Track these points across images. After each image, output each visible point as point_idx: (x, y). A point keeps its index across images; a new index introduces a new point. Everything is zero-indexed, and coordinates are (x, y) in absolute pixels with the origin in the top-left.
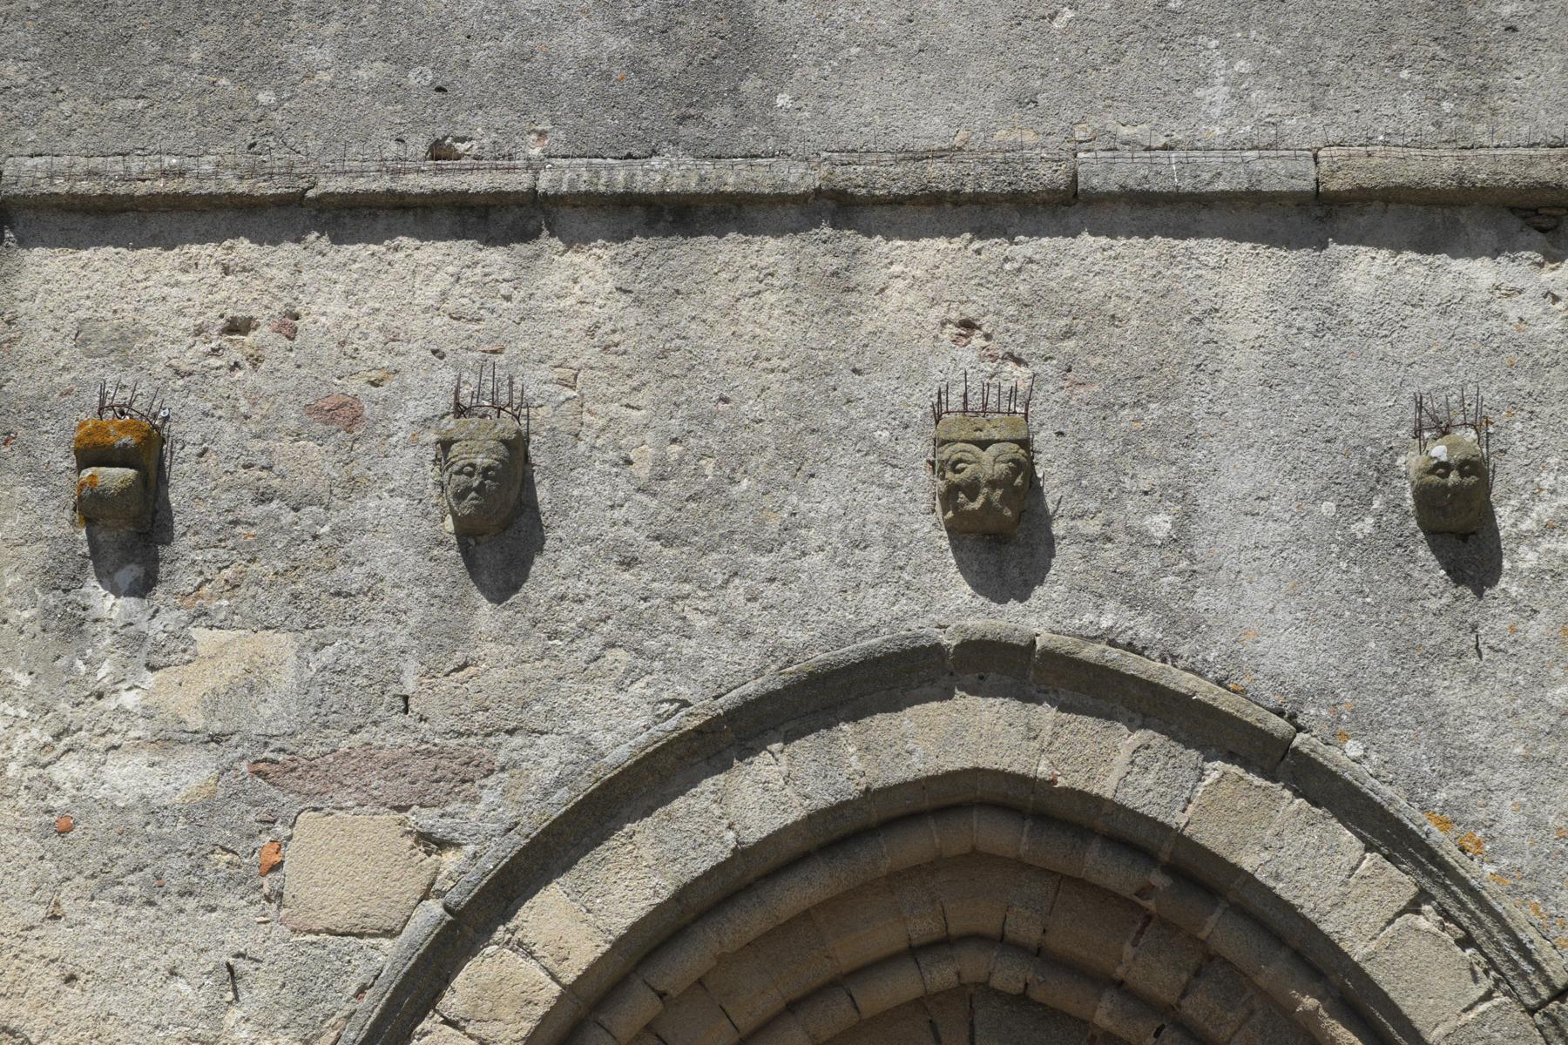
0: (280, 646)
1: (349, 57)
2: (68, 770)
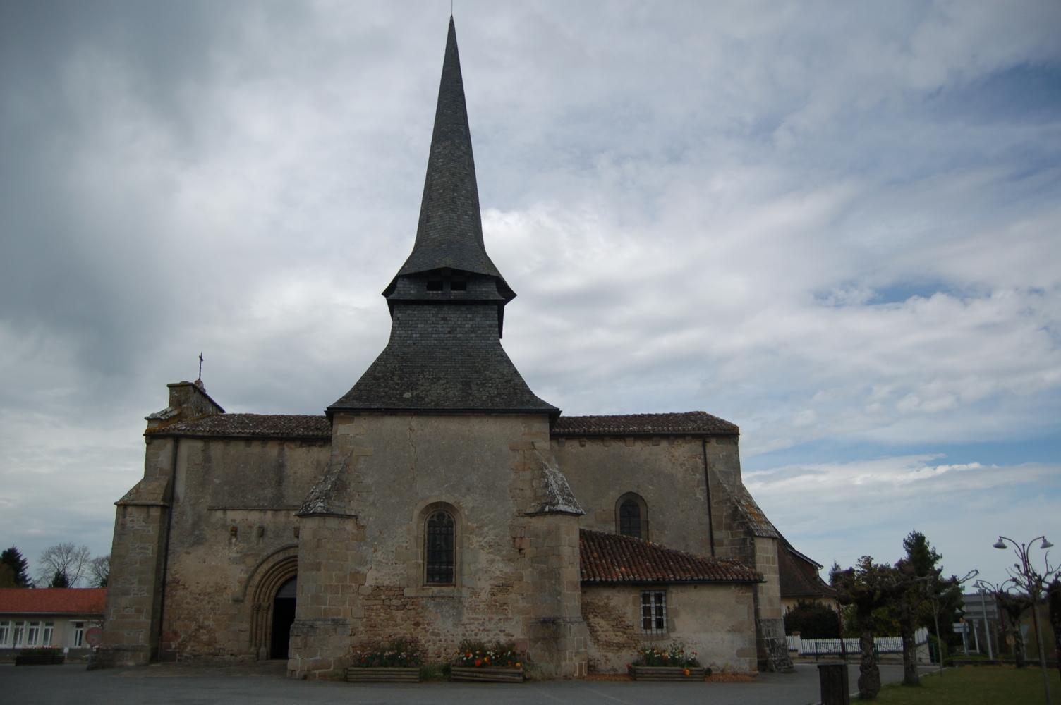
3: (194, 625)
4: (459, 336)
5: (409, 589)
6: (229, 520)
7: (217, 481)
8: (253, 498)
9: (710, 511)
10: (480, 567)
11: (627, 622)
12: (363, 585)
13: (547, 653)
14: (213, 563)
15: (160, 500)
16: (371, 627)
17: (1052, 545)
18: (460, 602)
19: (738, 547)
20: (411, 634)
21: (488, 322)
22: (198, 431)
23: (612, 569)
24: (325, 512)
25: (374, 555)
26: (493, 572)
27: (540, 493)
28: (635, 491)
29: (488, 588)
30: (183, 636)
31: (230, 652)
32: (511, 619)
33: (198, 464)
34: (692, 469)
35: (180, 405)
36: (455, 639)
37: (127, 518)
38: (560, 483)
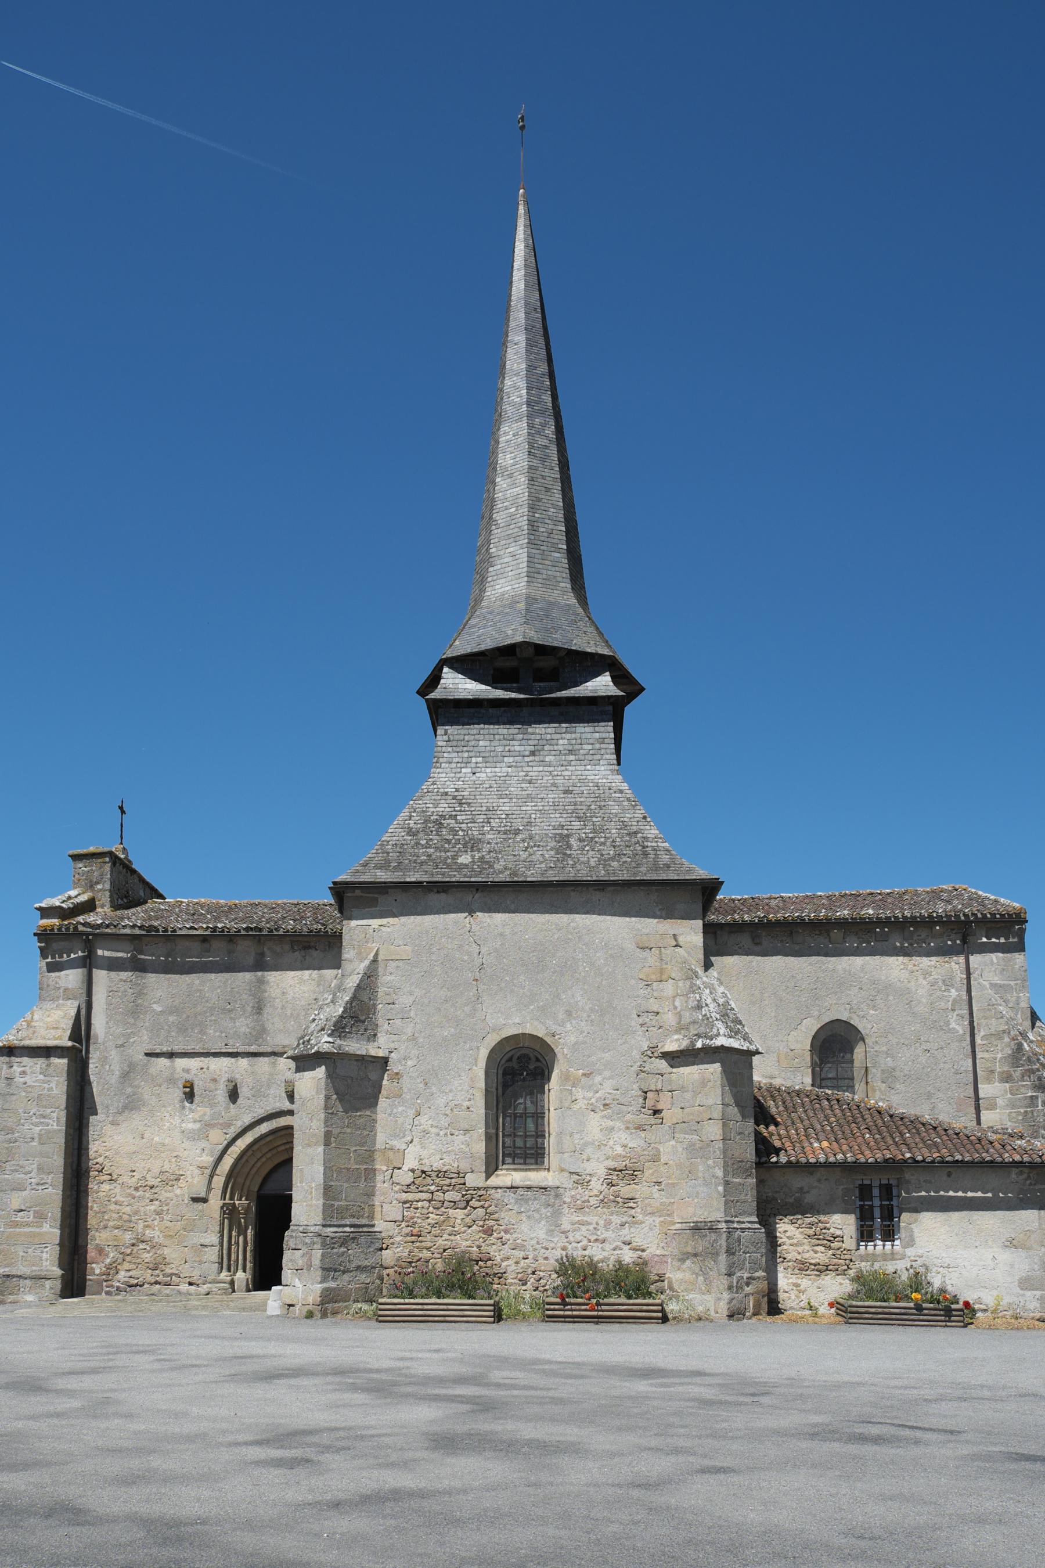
0: (208, 1110)
1: (215, 1032)
2: (183, 1125)
3: (128, 1237)
4: (547, 759)
6: (179, 1070)
7: (158, 1008)
8: (217, 1034)
9: (974, 1052)
11: (832, 1230)
12: (399, 1168)
13: (701, 1278)
14: (156, 1139)
15: (67, 1038)
16: (412, 1235)
17: (69, 856)
18: (557, 1196)
19: (1022, 1111)
20: (479, 1247)
21: (597, 735)
22: (124, 927)
23: (806, 1144)
25: (416, 1122)
26: (611, 1148)
27: (687, 1017)
29: (602, 1172)
30: (112, 1255)
31: (188, 1280)
32: (642, 1222)
34: (944, 981)
35: (91, 887)
36: (550, 1256)
38: (721, 1001)
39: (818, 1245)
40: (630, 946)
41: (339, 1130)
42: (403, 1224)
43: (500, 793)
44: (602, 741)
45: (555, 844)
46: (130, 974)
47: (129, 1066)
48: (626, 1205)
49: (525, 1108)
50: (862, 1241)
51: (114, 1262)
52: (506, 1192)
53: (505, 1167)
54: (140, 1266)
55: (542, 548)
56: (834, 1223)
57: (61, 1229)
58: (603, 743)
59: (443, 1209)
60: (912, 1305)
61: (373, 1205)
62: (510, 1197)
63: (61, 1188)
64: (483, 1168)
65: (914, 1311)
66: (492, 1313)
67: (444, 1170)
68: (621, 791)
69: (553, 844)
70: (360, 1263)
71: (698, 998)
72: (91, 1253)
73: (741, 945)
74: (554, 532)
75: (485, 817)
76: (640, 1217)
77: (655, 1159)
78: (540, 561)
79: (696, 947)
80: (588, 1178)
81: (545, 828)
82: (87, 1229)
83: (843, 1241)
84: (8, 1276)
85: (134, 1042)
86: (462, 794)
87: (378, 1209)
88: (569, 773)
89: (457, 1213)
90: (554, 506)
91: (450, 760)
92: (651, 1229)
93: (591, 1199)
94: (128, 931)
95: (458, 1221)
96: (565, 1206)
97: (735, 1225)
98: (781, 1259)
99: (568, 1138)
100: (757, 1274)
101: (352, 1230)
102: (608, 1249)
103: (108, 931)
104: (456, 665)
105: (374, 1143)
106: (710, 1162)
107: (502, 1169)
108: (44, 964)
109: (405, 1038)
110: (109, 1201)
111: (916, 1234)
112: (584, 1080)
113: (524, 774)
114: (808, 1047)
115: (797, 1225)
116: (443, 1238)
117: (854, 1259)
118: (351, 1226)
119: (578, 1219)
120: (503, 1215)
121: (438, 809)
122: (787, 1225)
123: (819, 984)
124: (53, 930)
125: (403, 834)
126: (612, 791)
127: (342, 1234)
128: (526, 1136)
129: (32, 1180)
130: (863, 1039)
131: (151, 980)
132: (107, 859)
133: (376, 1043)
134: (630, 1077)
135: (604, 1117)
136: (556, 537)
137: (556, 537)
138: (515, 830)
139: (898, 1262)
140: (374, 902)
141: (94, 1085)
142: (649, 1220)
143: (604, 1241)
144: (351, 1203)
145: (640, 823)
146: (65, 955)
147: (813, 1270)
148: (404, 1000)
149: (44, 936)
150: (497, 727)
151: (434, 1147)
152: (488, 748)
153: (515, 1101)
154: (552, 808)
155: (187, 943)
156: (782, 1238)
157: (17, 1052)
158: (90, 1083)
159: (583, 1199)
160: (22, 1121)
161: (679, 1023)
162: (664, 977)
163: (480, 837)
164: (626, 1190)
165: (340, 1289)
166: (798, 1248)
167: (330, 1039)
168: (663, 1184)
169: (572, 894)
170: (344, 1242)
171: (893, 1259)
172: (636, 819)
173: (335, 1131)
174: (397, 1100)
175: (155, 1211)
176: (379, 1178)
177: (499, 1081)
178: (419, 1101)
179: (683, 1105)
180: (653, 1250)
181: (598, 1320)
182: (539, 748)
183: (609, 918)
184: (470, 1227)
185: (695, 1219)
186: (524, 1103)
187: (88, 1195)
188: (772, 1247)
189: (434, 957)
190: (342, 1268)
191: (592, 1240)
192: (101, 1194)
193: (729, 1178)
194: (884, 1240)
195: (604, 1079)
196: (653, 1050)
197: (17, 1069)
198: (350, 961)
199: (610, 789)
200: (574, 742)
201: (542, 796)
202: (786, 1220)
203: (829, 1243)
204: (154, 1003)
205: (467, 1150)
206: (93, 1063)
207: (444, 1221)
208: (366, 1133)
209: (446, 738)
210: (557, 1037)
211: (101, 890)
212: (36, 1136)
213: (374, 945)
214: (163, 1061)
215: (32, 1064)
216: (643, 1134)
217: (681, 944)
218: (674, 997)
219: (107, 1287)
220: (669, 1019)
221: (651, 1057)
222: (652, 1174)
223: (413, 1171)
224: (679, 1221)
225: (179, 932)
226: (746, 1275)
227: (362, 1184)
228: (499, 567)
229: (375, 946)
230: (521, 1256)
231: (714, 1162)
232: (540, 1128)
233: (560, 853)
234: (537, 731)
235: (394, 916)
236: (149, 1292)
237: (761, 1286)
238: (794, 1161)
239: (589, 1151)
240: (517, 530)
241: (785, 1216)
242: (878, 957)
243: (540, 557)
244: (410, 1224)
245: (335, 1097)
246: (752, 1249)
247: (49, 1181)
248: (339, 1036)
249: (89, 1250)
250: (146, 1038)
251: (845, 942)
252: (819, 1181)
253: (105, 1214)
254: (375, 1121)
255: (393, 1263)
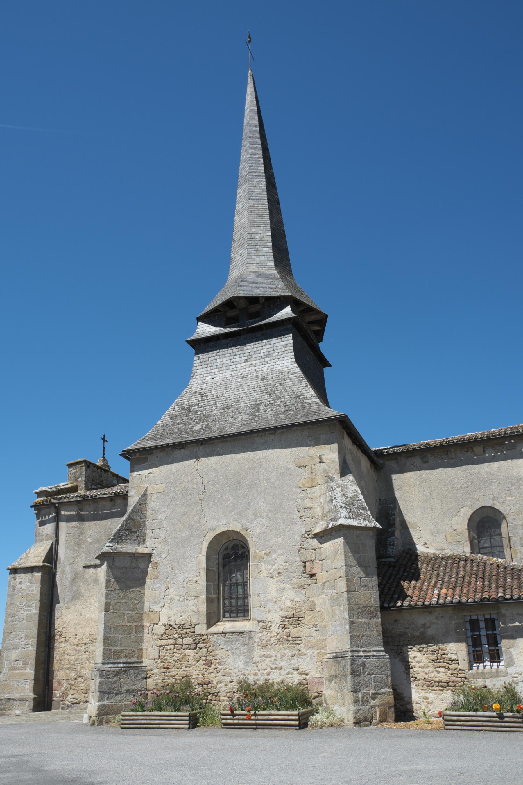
3: (73, 674)
4: (254, 362)
5: (200, 626)
7: (89, 540)
10: (270, 597)
11: (449, 655)
12: (157, 624)
14: (88, 616)
16: (164, 668)
18: (250, 637)
20: (203, 675)
21: (283, 343)
24: (112, 551)
25: (167, 593)
27: (327, 508)
28: (490, 505)
32: (305, 654)
33: (74, 527)
35: (76, 480)
37: (17, 580)
39: (440, 667)
40: (292, 466)
41: (116, 601)
42: (159, 661)
43: (225, 386)
44: (286, 346)
45: (250, 410)
46: (77, 523)
47: (75, 575)
48: (294, 642)
49: (237, 580)
50: (475, 663)
51: (66, 690)
52: (219, 636)
53: (224, 619)
54: (79, 691)
55: (257, 247)
56: (450, 650)
57: (35, 671)
58: (286, 347)
59: (182, 650)
60: (494, 714)
61: (142, 649)
62: (221, 640)
63: (36, 646)
64: (205, 621)
65: (497, 719)
66: (187, 722)
67: (183, 623)
68: (295, 373)
69: (249, 411)
70: (129, 688)
71: (331, 494)
72: (55, 685)
73: (415, 464)
74: (264, 237)
75: (214, 401)
76: (304, 651)
77: (312, 608)
78: (255, 254)
79: (334, 462)
80: (270, 624)
81: (247, 402)
82: (53, 670)
83: (458, 663)
84: (8, 699)
85: (78, 561)
86: (204, 391)
87: (144, 651)
88: (266, 368)
89: (190, 652)
90: (264, 223)
91: (200, 373)
92: (311, 659)
93: (271, 638)
94: (74, 499)
95: (191, 658)
96: (256, 644)
97: (361, 654)
98: (414, 679)
99: (256, 597)
100: (383, 691)
101: (125, 665)
102: (283, 674)
103: (65, 500)
104: (205, 320)
105: (143, 608)
106: (342, 608)
107: (221, 621)
108: (38, 522)
109: (160, 540)
110: (64, 653)
111: (515, 656)
112: (266, 557)
113: (240, 373)
114: (466, 527)
115: (423, 652)
116: (182, 669)
117: (467, 677)
118: (124, 663)
119: (263, 653)
120: (217, 652)
121: (190, 402)
122: (415, 653)
123: (469, 484)
124: (40, 503)
125: (168, 419)
126: (289, 374)
127: (115, 669)
128: (237, 598)
129: (22, 643)
130: (504, 518)
131: (87, 525)
132: (83, 465)
133: (145, 546)
134: (294, 553)
135: (279, 581)
136: (265, 239)
137: (265, 239)
138: (230, 406)
139: (501, 678)
140: (145, 460)
141: (59, 587)
142: (310, 652)
143: (281, 668)
144: (125, 648)
145: (303, 390)
146: (47, 517)
147: (437, 686)
148: (161, 517)
149: (37, 507)
150: (226, 350)
151: (177, 609)
152: (221, 363)
153: (230, 576)
154: (253, 390)
155: (104, 503)
156: (413, 663)
157: (18, 571)
158: (56, 586)
159: (266, 639)
160: (19, 609)
161: (323, 513)
162: (314, 484)
163: (209, 413)
164: (294, 631)
165: (113, 706)
166: (425, 670)
167: (110, 545)
168: (318, 625)
169: (256, 438)
170: (117, 674)
171: (498, 676)
172: (301, 388)
173: (113, 602)
174: (156, 580)
175: (86, 658)
176: (146, 631)
177: (220, 562)
178: (168, 580)
179: (327, 569)
180: (314, 674)
181: (256, 727)
182: (250, 357)
183: (279, 450)
184: (198, 661)
185: (337, 650)
186: (237, 576)
187: (54, 650)
188: (406, 669)
189: (177, 489)
190: (115, 692)
191: (273, 668)
192: (61, 649)
193: (355, 619)
194: (492, 660)
195: (278, 555)
196: (308, 533)
197: (18, 580)
198: (133, 496)
199: (288, 373)
200: (269, 350)
201: (248, 384)
202: (415, 649)
203: (448, 665)
204: (88, 538)
205: (196, 609)
206: (59, 574)
207: (182, 658)
208: (136, 602)
209: (198, 361)
210: (248, 531)
211: (80, 481)
212: (25, 617)
213: (145, 485)
214: (92, 570)
215: (25, 577)
216: (303, 591)
217: (324, 461)
218: (320, 496)
219: (62, 704)
220: (318, 511)
221: (307, 538)
222: (311, 619)
223: (165, 625)
224: (329, 652)
225: (98, 497)
226: (371, 692)
227: (133, 636)
228: (235, 263)
229: (145, 486)
230: (229, 680)
231: (344, 608)
232: (246, 593)
233: (252, 415)
234: (249, 347)
235: (157, 466)
236: (82, 708)
237: (387, 700)
238: (413, 604)
239: (270, 605)
240: (243, 240)
241: (414, 646)
242: (510, 460)
243: (255, 252)
244: (163, 660)
245: (113, 580)
246: (377, 671)
247: (30, 643)
248: (117, 542)
249: (54, 683)
250: (84, 558)
251: (486, 453)
252: (437, 618)
253: (62, 661)
254: (143, 594)
255: (153, 687)
